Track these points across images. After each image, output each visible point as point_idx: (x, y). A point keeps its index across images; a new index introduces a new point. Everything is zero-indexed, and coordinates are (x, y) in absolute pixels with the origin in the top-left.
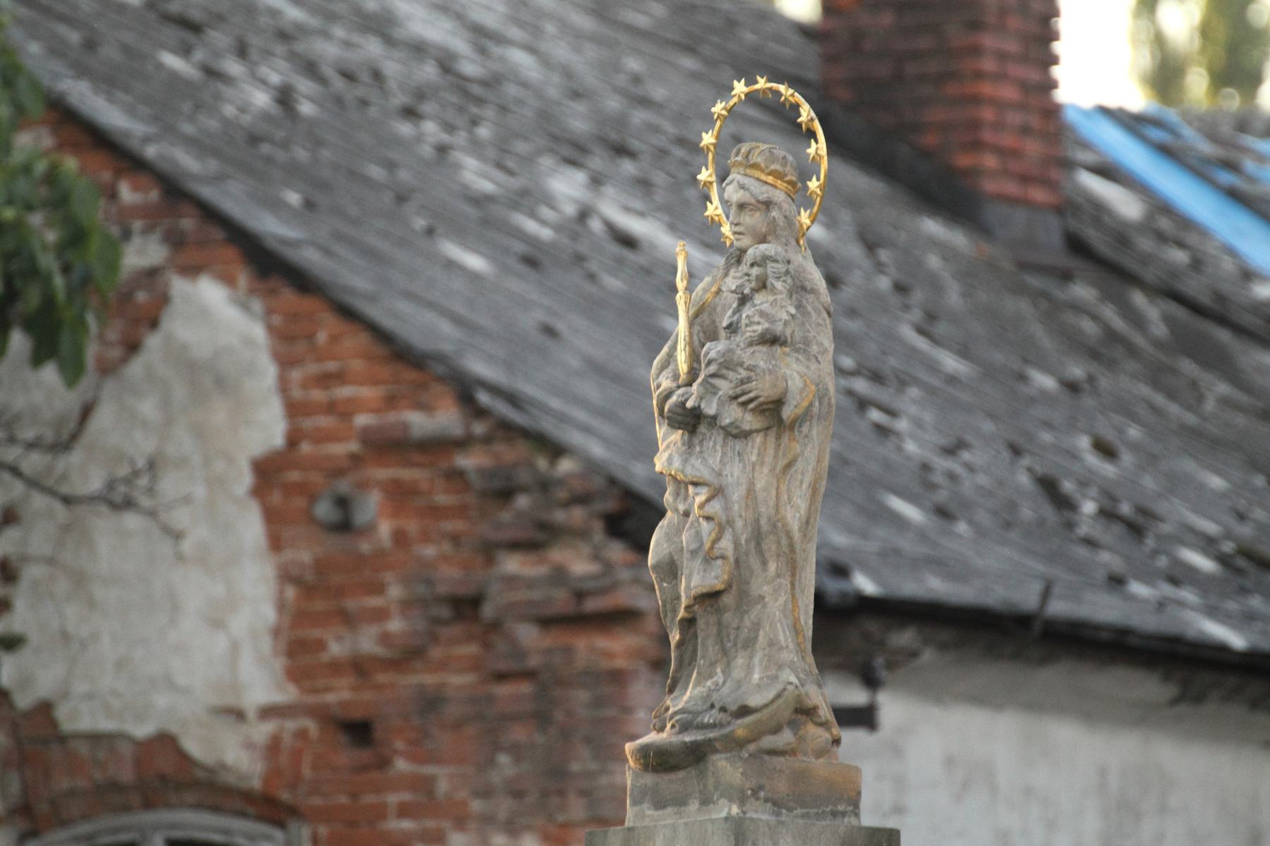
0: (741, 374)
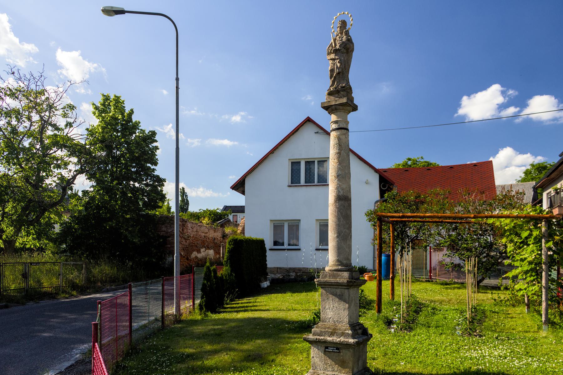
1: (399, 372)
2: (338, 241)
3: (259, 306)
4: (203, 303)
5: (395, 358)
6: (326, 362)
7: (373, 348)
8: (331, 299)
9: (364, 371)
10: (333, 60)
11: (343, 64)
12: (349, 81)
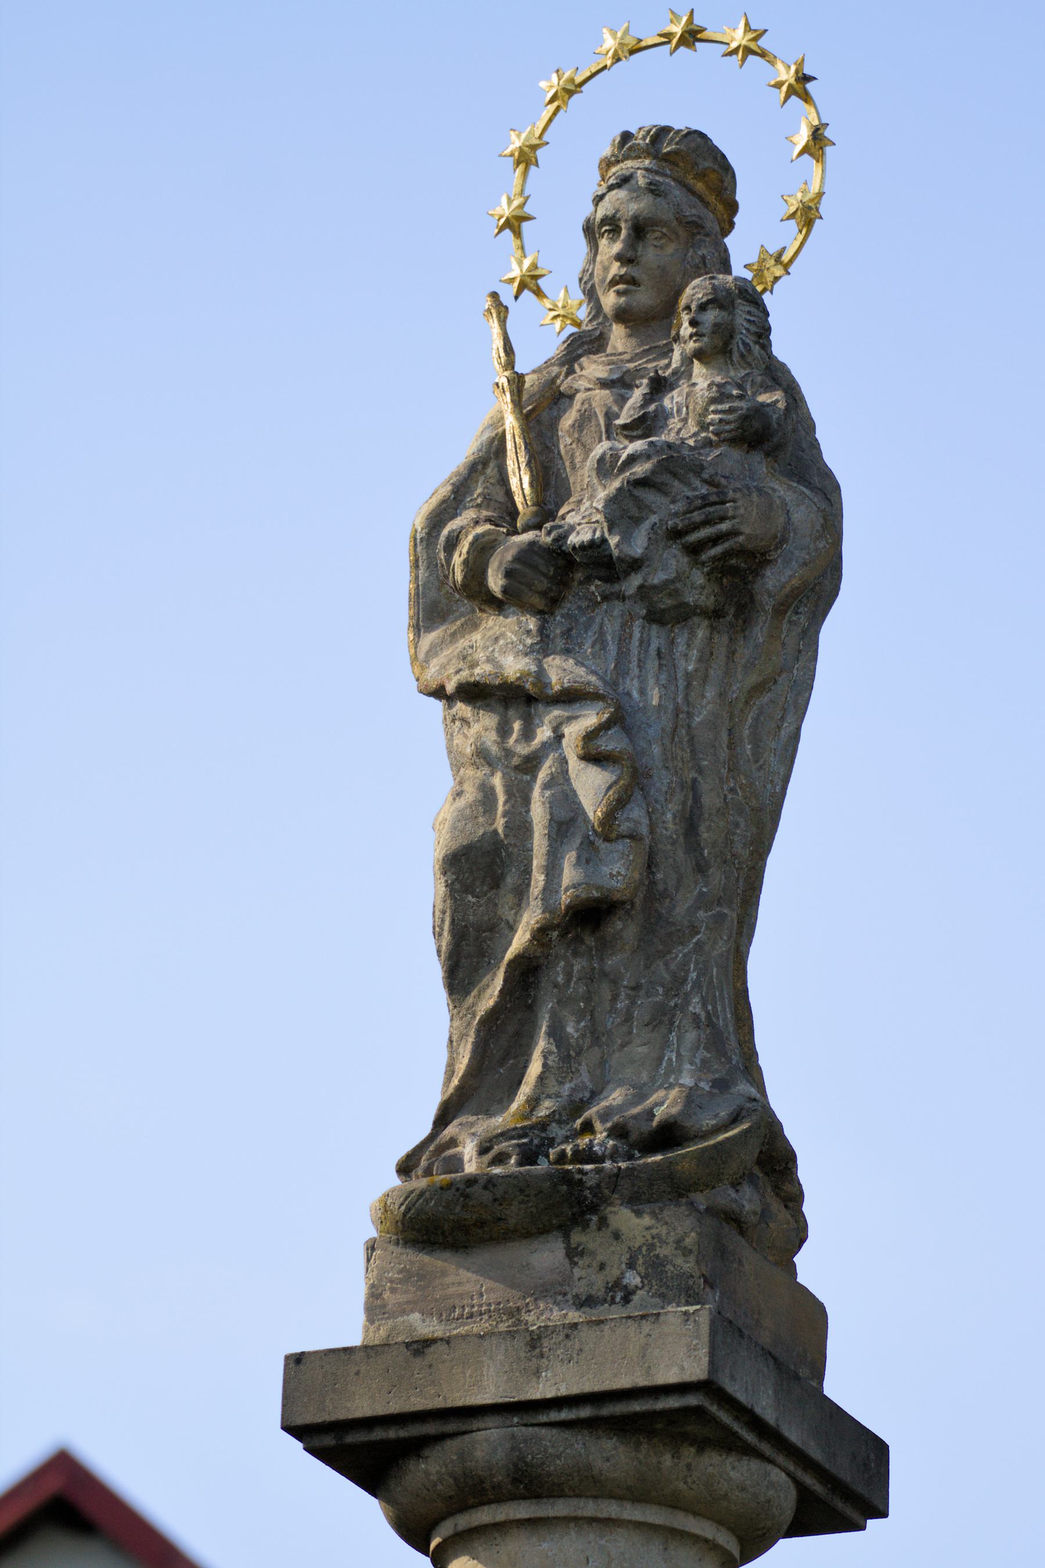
0: (695, 489)
11: (662, 781)
12: (750, 1056)
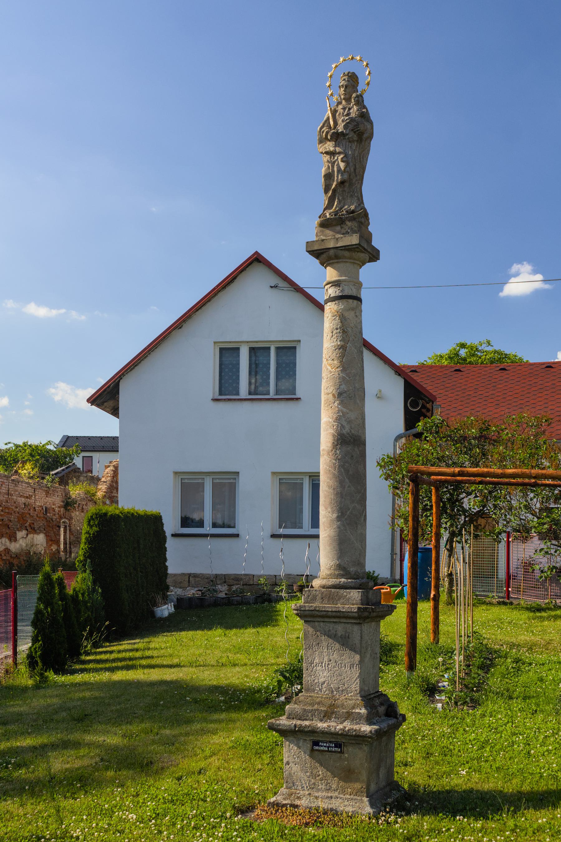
1: (456, 788)
2: (339, 527)
3: (158, 657)
4: (36, 652)
5: (449, 763)
6: (314, 772)
7: (403, 742)
8: (325, 644)
9: (388, 789)
10: (331, 154)
11: (351, 164)
12: (362, 201)
